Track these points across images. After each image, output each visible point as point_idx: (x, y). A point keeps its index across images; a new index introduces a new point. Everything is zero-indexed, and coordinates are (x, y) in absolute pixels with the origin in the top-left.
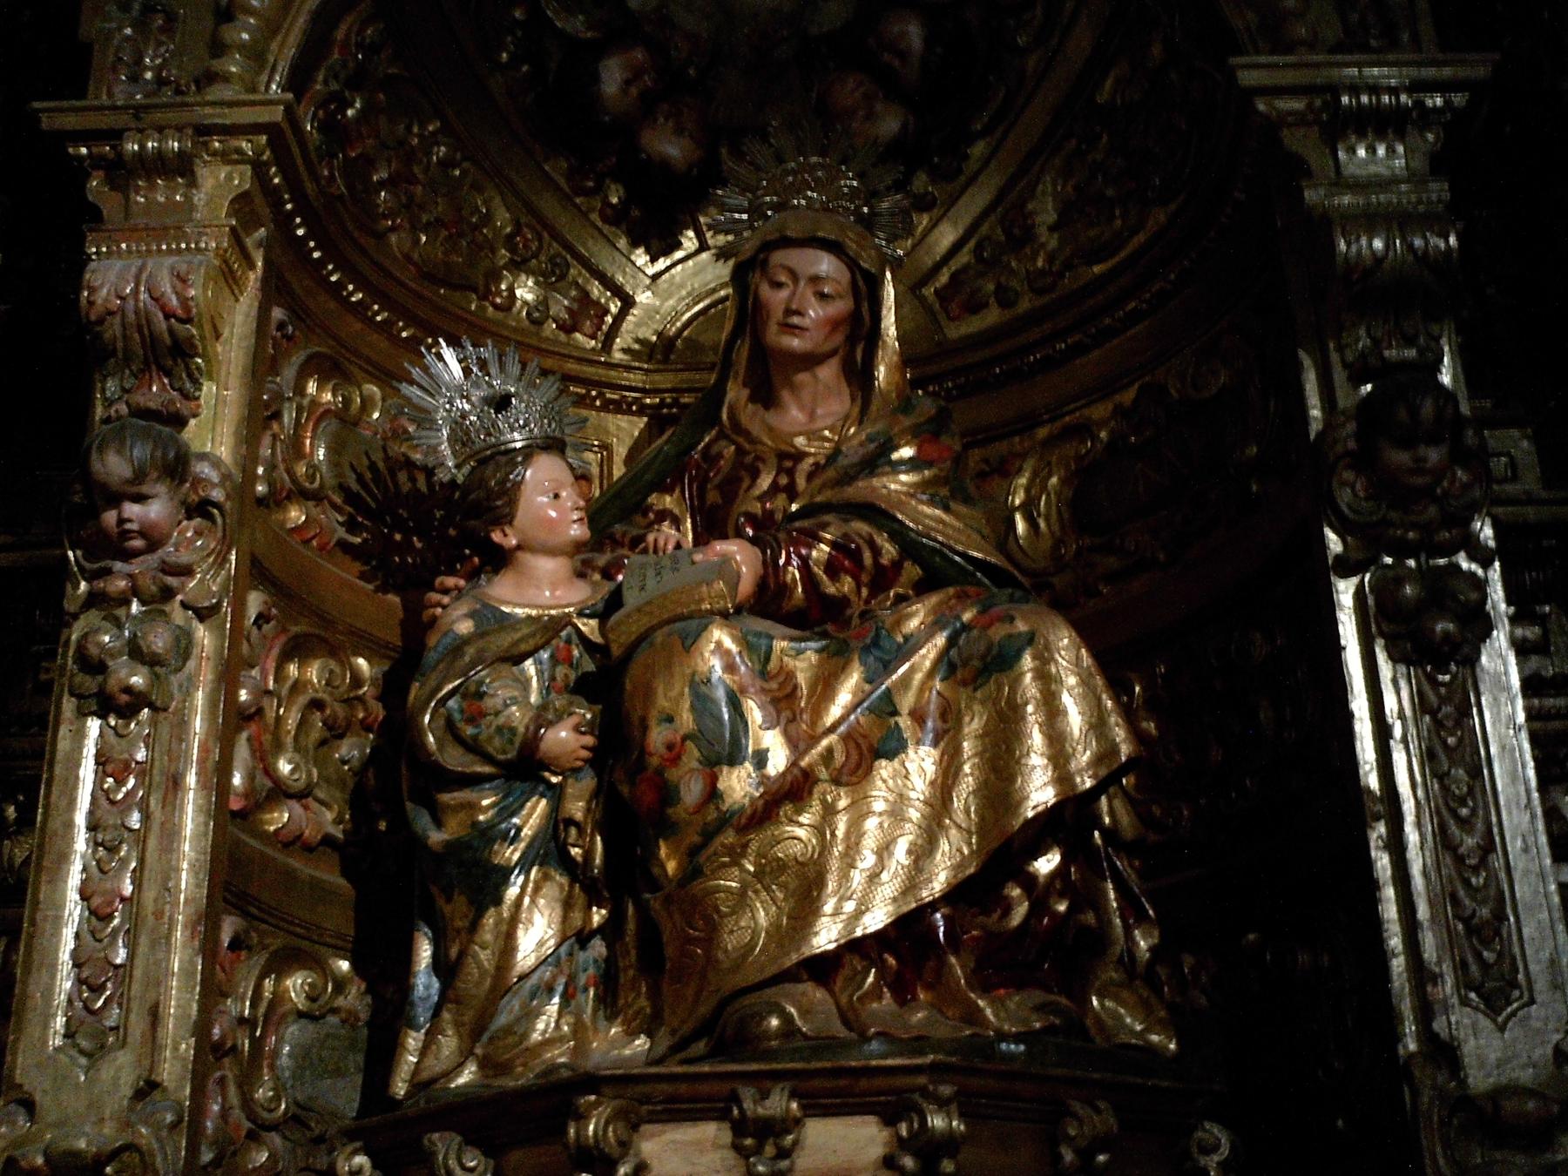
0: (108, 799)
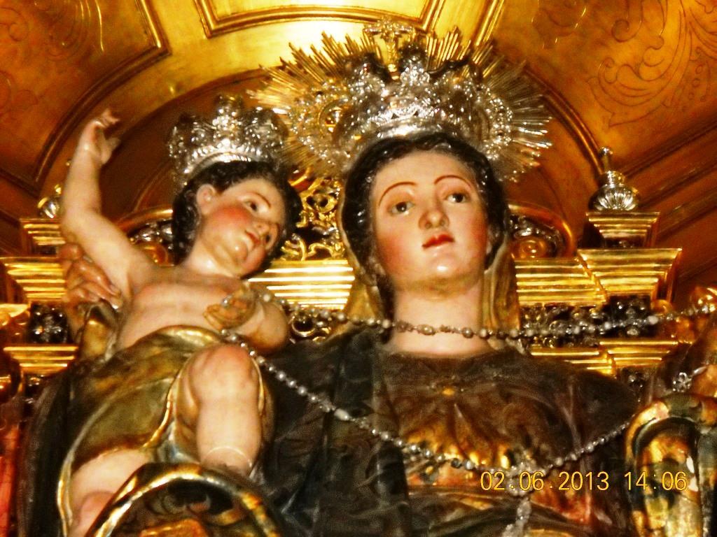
0: (551, 20)
